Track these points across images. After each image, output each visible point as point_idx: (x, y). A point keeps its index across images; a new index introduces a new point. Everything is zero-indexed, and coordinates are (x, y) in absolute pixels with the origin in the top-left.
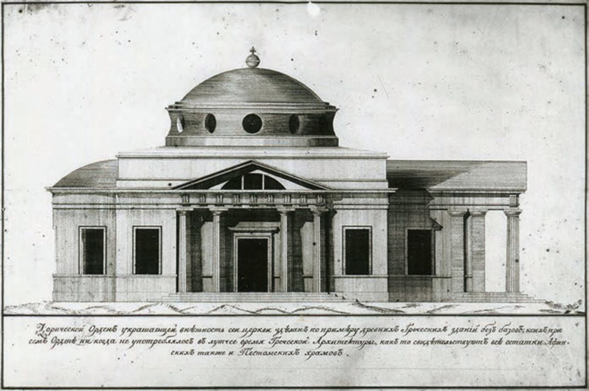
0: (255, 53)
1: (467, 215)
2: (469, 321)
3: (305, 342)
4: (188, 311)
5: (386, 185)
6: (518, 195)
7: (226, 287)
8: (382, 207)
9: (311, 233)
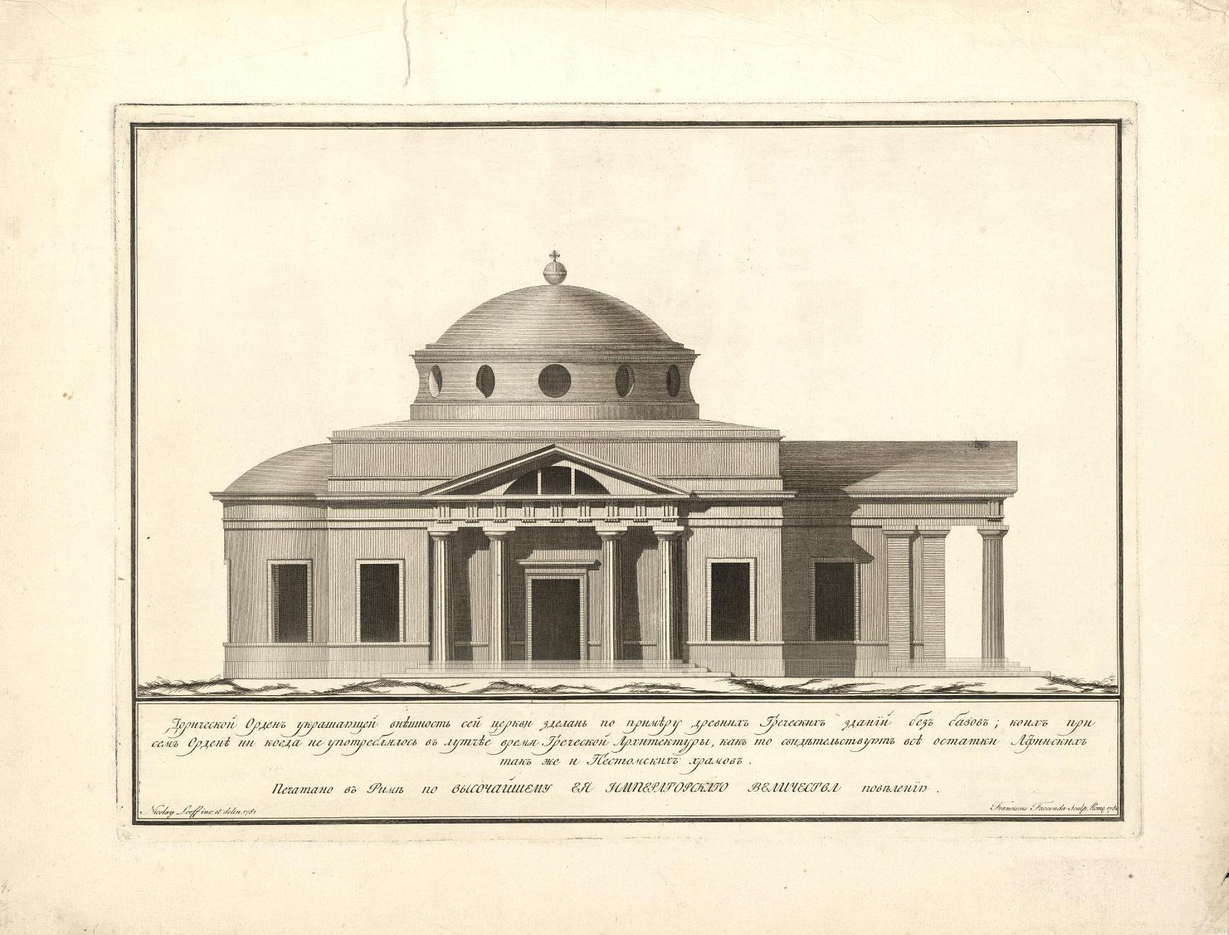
0: (558, 260)
1: (915, 535)
2: (658, 91)
3: (885, 723)
4: (457, 690)
5: (778, 485)
6: (1001, 501)
7: (512, 652)
8: (771, 523)
9: (654, 568)
